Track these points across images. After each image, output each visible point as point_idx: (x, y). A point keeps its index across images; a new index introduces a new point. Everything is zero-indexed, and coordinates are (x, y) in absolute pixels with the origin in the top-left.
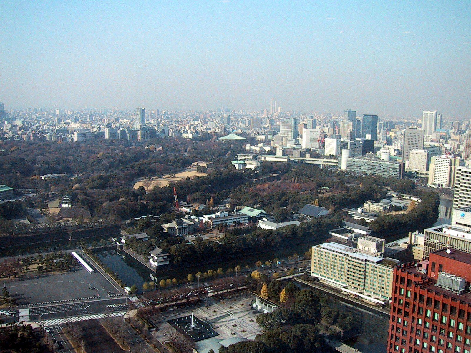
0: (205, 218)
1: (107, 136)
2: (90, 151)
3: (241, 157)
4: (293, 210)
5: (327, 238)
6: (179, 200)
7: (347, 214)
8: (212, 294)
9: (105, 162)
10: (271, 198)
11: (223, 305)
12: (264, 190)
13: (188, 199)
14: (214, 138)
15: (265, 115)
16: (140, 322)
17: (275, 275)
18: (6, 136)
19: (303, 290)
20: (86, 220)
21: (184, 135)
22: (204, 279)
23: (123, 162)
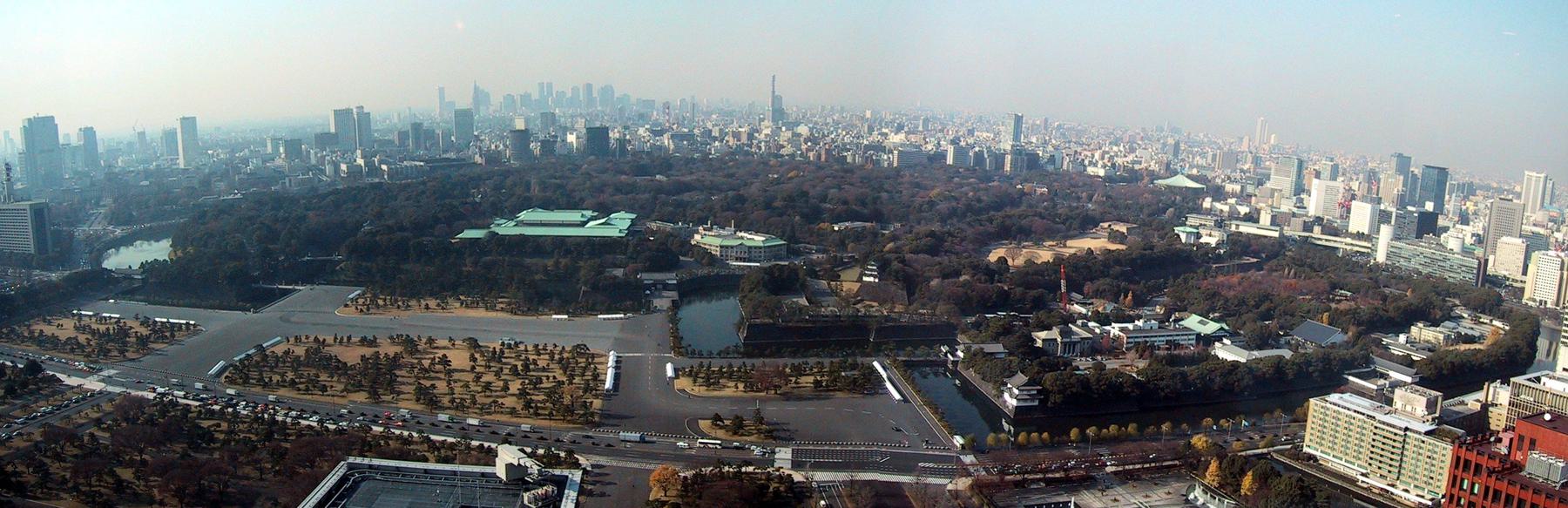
0: (1115, 329)
1: (950, 160)
2: (918, 185)
3: (1193, 220)
4: (1281, 328)
5: (1338, 385)
6: (1069, 290)
7: (1379, 343)
8: (1114, 469)
9: (943, 207)
10: (1242, 302)
11: (1131, 490)
12: (1230, 287)
13: (1086, 289)
14: (1146, 179)
15: (1244, 147)
16: (975, 500)
17: (1236, 445)
18: (783, 152)
19: (1286, 475)
20: (899, 308)
21: (1091, 170)
22: (1100, 441)
23: (972, 210)
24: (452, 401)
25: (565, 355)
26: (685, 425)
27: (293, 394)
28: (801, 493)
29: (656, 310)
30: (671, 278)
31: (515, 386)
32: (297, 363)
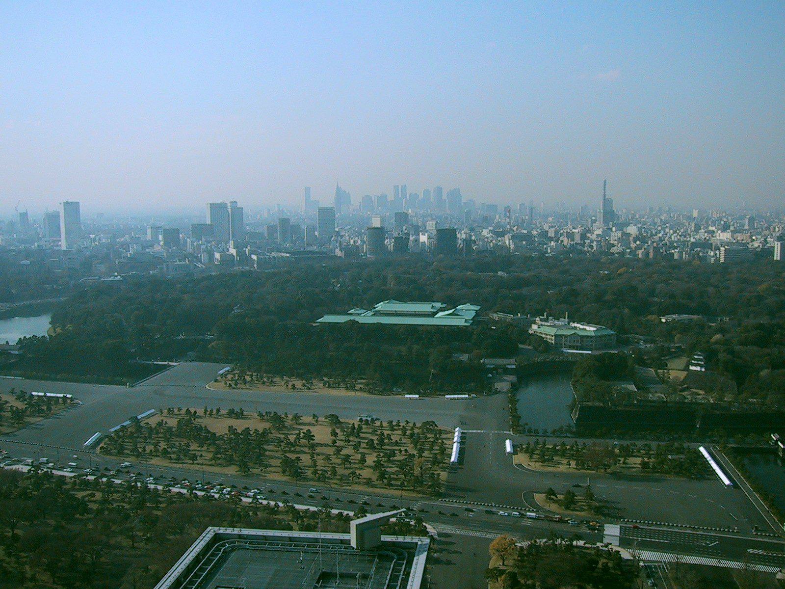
1: (777, 256)
20: (728, 398)
24: (315, 472)
25: (416, 431)
26: (518, 497)
27: (165, 463)
28: (629, 571)
29: (497, 392)
30: (511, 363)
31: (371, 460)
32: (169, 434)
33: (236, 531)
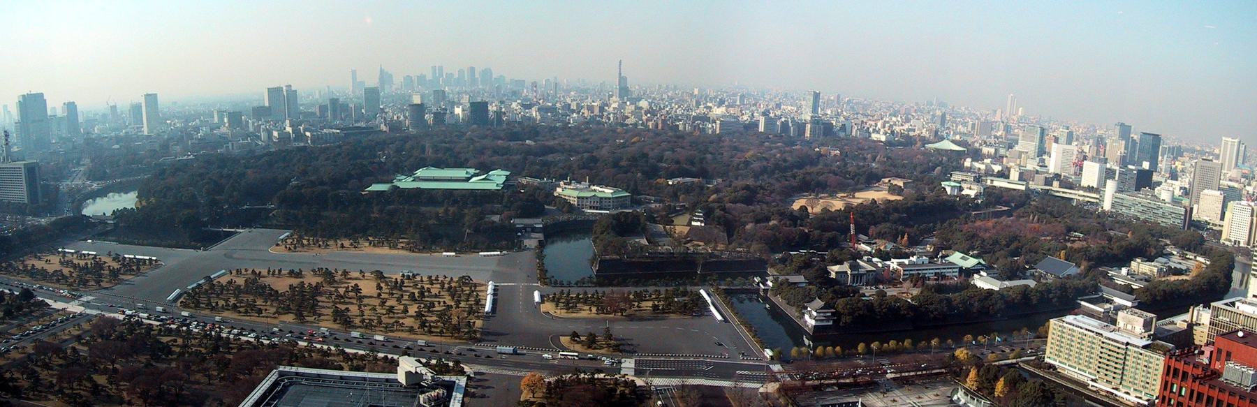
0: (894, 264)
1: (761, 129)
2: (736, 148)
3: (956, 176)
4: (1027, 263)
5: (1073, 309)
6: (857, 232)
7: (1105, 275)
8: (893, 376)
9: (756, 165)
10: (996, 242)
11: (907, 392)
12: (986, 230)
13: (870, 231)
14: (919, 144)
15: (998, 118)
16: (782, 401)
17: (991, 357)
18: (628, 121)
19: (1031, 381)
20: (720, 247)
21: (874, 136)
22: (882, 353)
23: (780, 168)
24: (363, 321)
25: (453, 285)
26: (549, 341)
27: (235, 316)
28: (642, 395)
29: (526, 249)
30: (538, 223)
31: (413, 310)
32: (238, 291)
33: (294, 369)
